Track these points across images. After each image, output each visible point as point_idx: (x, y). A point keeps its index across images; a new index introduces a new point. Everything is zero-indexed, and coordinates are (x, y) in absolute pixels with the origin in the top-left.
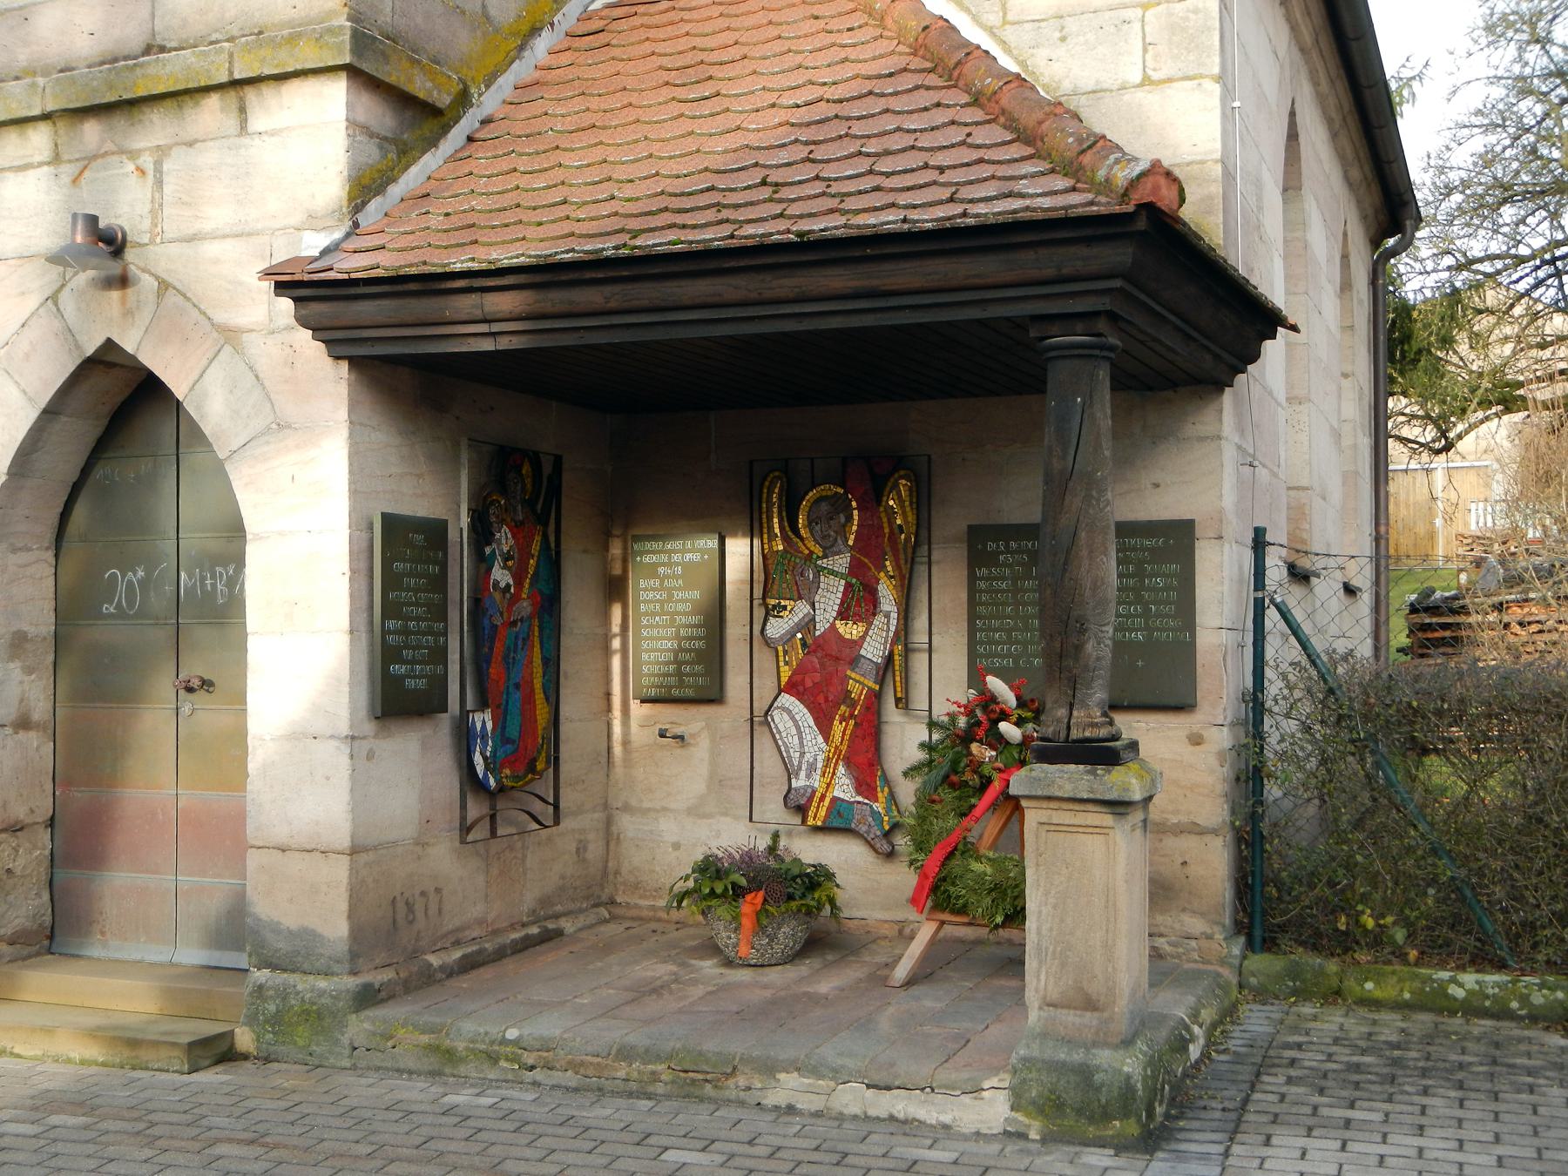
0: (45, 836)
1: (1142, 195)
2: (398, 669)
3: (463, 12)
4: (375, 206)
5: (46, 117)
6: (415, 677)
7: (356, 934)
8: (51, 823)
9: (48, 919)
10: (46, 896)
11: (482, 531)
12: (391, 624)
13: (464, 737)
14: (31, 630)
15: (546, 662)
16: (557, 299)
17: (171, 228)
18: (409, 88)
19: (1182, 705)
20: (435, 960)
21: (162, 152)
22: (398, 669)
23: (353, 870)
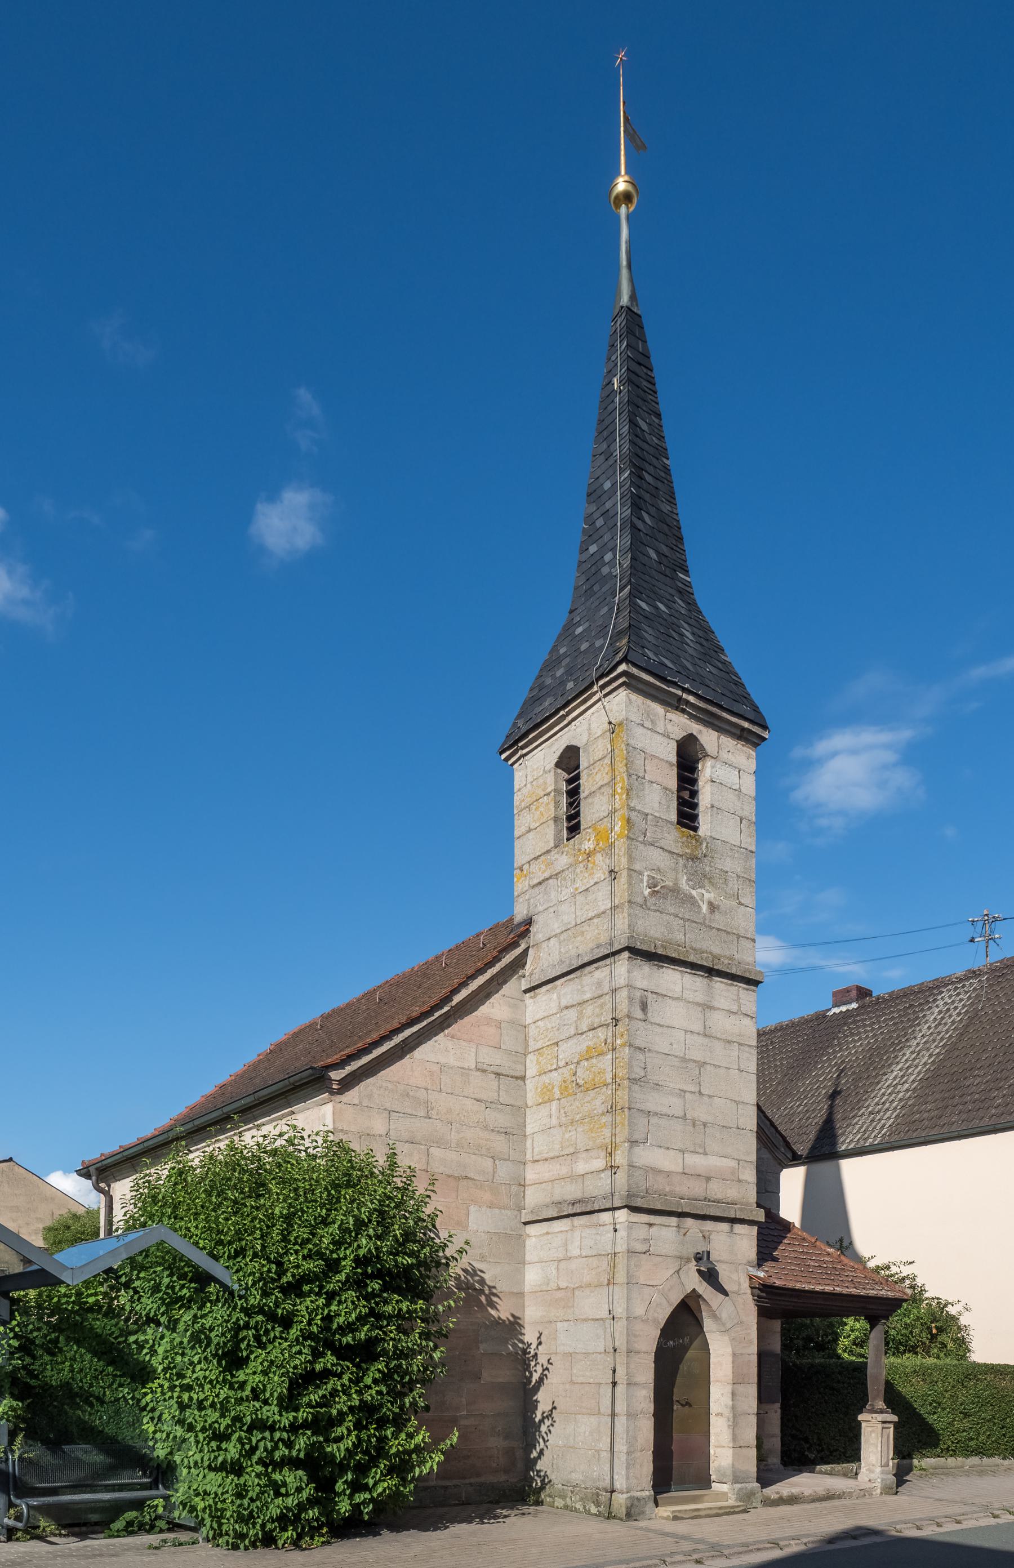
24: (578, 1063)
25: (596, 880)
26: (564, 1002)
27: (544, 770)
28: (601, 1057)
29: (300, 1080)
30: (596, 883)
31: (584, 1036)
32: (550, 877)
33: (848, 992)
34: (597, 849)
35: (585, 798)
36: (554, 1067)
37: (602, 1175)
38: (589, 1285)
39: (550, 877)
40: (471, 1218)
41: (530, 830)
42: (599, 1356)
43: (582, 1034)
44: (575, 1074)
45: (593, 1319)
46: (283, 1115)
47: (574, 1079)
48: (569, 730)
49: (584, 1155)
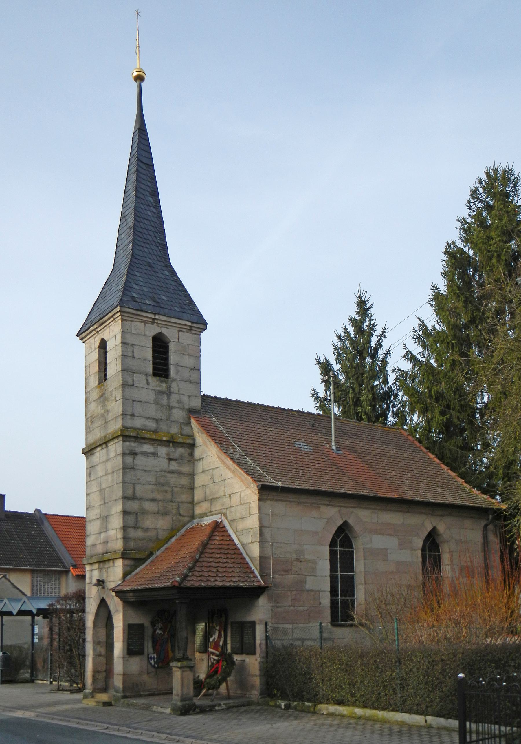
0: (105, 673)
1: (173, 584)
2: (131, 647)
3: (151, 540)
4: (128, 577)
5: (97, 562)
6: (466, 637)
7: (124, 687)
8: (106, 671)
9: (105, 687)
10: (104, 683)
11: (153, 624)
12: (130, 641)
13: (149, 658)
14: (102, 640)
15: (172, 646)
16: (137, 594)
17: (108, 580)
18: (136, 557)
19: (254, 653)
20: (142, 693)
21: (107, 568)
22: (131, 647)
23: (123, 678)
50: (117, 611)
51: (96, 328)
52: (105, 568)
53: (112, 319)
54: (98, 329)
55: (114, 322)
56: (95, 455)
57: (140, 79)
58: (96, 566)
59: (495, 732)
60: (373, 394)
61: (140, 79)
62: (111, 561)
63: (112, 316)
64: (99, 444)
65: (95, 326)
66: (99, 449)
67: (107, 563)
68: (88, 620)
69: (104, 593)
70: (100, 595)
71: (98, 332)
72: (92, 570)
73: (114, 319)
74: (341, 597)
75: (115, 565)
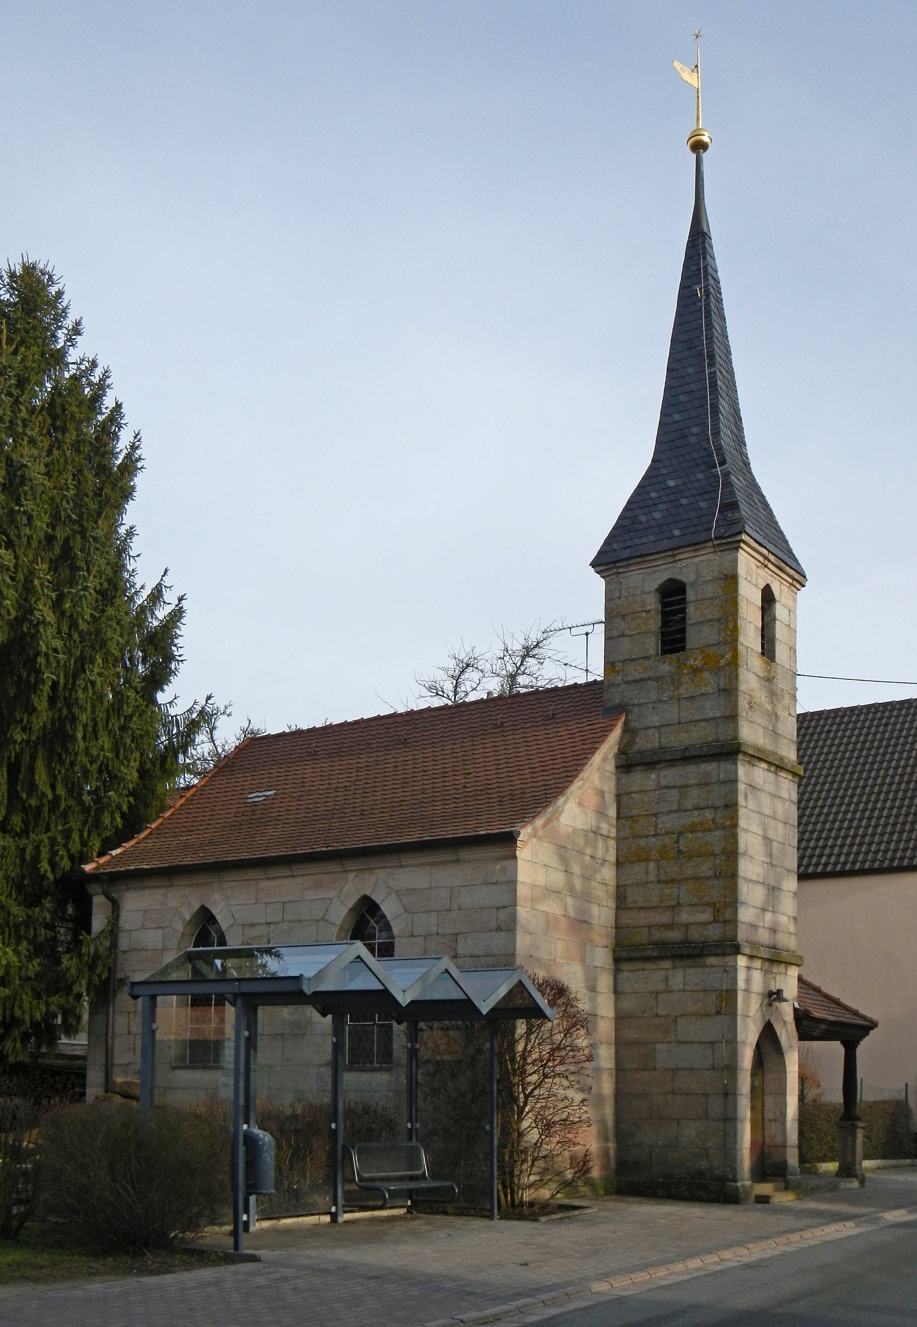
24: (680, 834)
25: (703, 691)
26: (664, 782)
27: (642, 590)
28: (707, 833)
29: (658, 559)
30: (702, 694)
31: (688, 813)
32: (650, 679)
33: (733, 836)
34: (705, 667)
35: (693, 625)
36: (653, 833)
37: (710, 927)
38: (695, 1014)
39: (650, 679)
40: (587, 955)
41: (623, 635)
42: (707, 1073)
43: (686, 811)
44: (677, 842)
45: (698, 1042)
46: (671, 606)
47: (676, 845)
48: (674, 567)
49: (688, 909)
50: (791, 1046)
51: (769, 561)
52: (772, 973)
53: (790, 580)
54: (770, 565)
55: (788, 585)
56: (755, 768)
57: (699, 147)
58: (758, 964)
59: (349, 1104)
60: (56, 511)
61: (699, 147)
62: (783, 965)
63: (794, 579)
64: (771, 759)
65: (772, 558)
66: (764, 765)
67: (776, 965)
68: (743, 1056)
69: (772, 1013)
70: (763, 1016)
71: (766, 566)
72: (748, 968)
73: (791, 584)
74: (379, 943)
75: (788, 973)
